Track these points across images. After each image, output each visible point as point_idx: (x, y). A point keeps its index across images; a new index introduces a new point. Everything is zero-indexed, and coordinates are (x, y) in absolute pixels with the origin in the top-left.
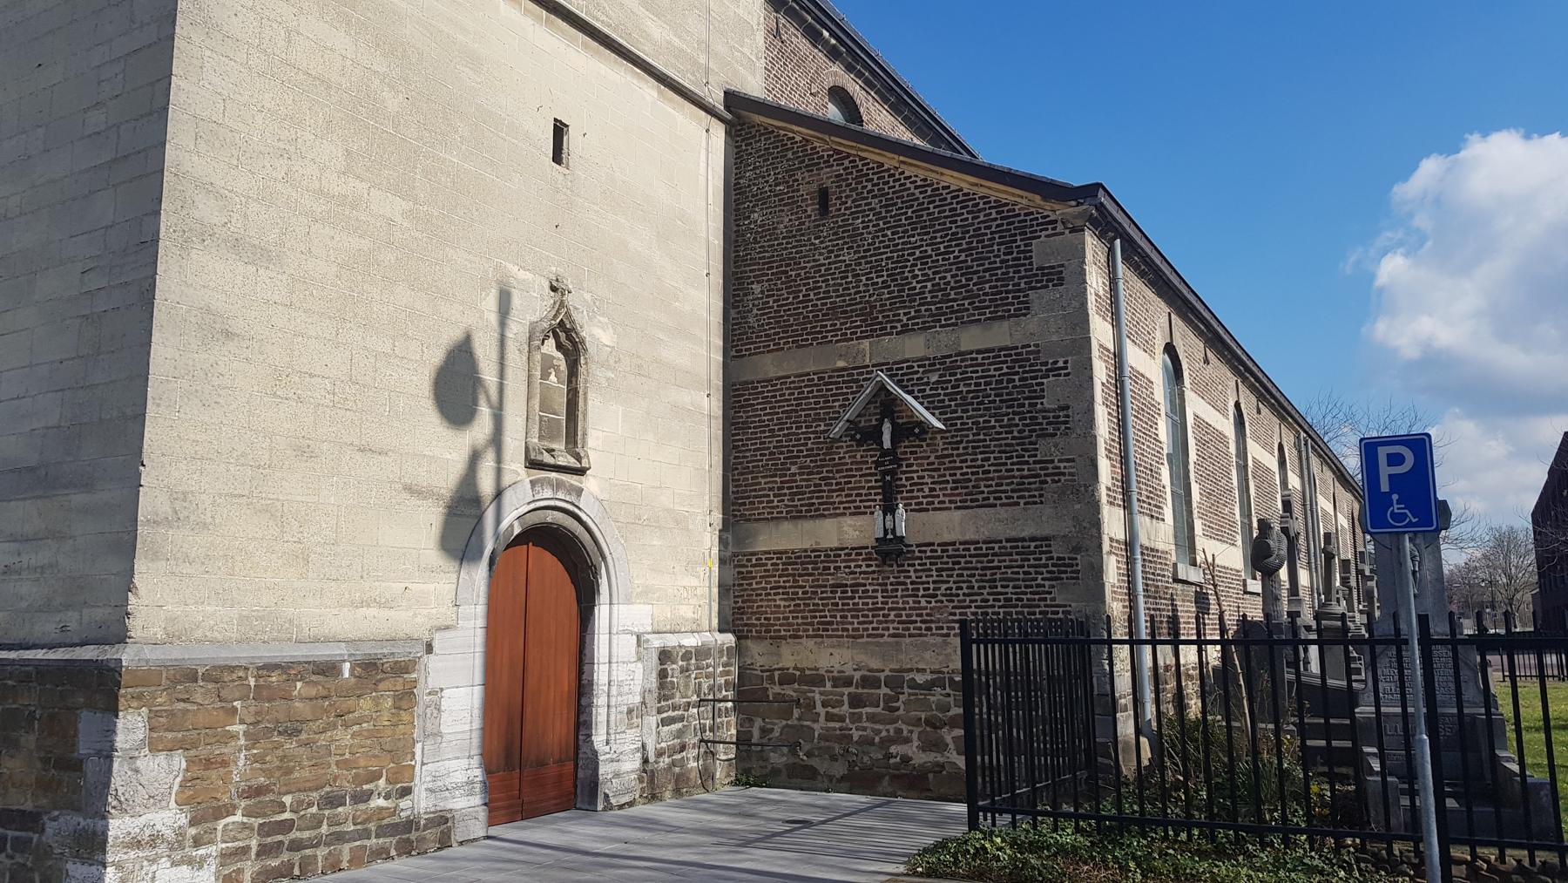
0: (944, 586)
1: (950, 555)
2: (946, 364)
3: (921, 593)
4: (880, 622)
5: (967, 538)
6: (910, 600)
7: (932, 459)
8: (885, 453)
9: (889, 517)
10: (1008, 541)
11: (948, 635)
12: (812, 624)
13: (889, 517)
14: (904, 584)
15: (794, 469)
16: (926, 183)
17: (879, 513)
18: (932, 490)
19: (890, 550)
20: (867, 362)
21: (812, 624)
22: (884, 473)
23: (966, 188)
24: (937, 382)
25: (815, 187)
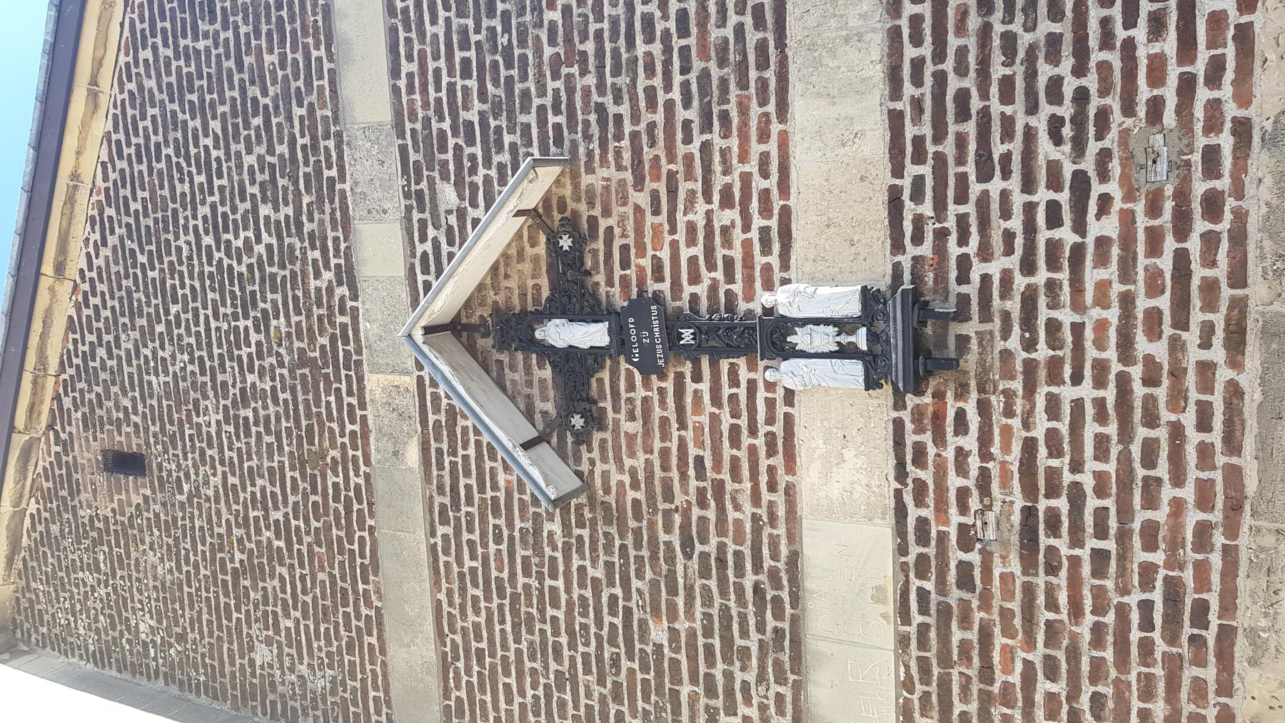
0: (1045, 148)
1: (935, 135)
2: (421, 160)
3: (1066, 235)
4: (1177, 399)
5: (877, 72)
6: (1092, 276)
7: (643, 199)
8: (620, 342)
9: (800, 339)
10: (896, 94)
11: (1242, 129)
12: (1174, 666)
13: (800, 339)
14: (1029, 300)
15: (659, 633)
16: (98, 221)
17: (789, 373)
18: (727, 201)
19: (909, 341)
20: (410, 382)
21: (1174, 666)
22: (672, 339)
23: (101, 125)
24: (459, 185)
25: (101, 479)
